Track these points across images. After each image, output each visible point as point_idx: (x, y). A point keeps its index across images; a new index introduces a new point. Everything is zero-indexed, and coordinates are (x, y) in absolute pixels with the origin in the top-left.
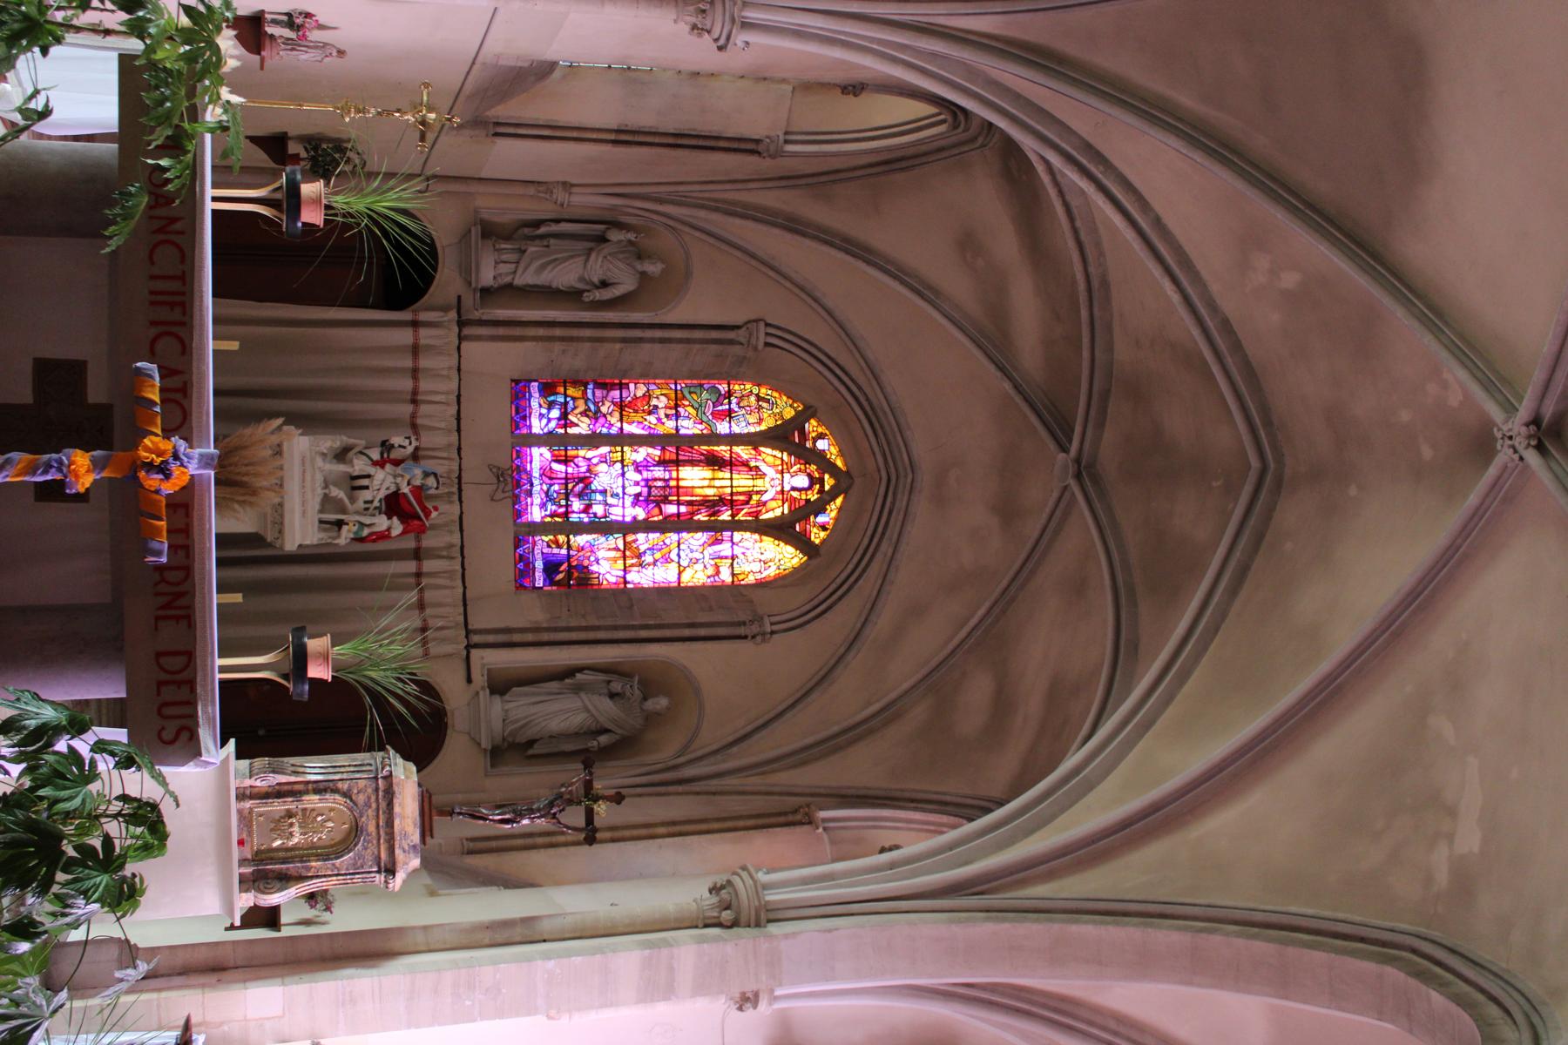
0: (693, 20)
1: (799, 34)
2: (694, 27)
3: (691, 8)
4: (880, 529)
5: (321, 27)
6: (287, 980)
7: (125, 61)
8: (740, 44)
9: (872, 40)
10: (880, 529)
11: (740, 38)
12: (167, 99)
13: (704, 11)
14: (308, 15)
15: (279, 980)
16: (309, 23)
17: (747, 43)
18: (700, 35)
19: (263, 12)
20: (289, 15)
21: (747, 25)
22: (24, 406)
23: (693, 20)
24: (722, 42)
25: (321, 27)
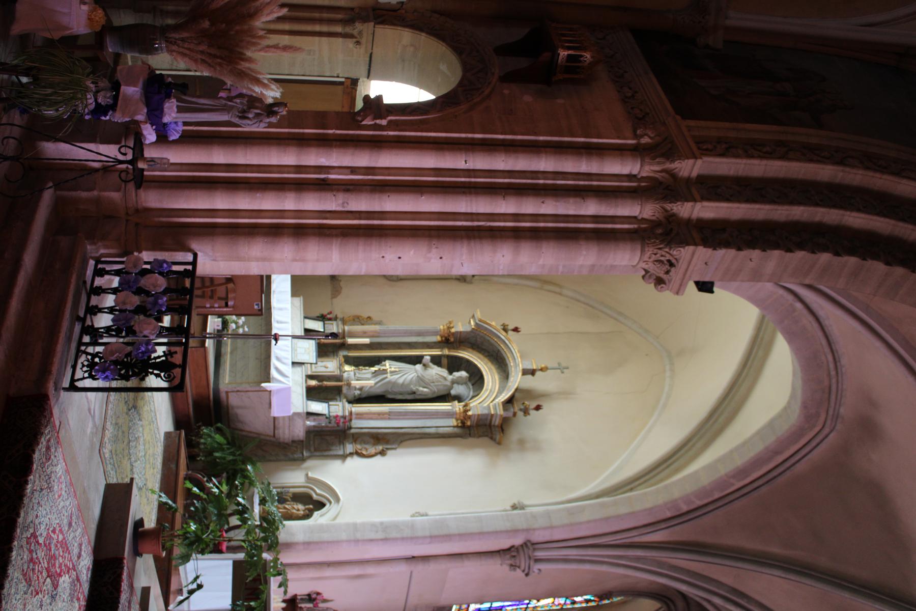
0: (509, 562)
1: (566, 560)
2: (511, 565)
3: (508, 556)
4: (813, 444)
5: (325, 601)
6: (472, 243)
7: (237, 565)
8: (536, 571)
9: (608, 556)
10: (813, 444)
11: (536, 567)
12: (255, 556)
13: (514, 556)
14: (318, 594)
15: (465, 242)
16: (318, 597)
17: (540, 570)
18: (515, 570)
19: (296, 595)
20: (309, 595)
21: (537, 560)
22: (161, 118)
23: (509, 562)
24: (526, 571)
25: (325, 601)
